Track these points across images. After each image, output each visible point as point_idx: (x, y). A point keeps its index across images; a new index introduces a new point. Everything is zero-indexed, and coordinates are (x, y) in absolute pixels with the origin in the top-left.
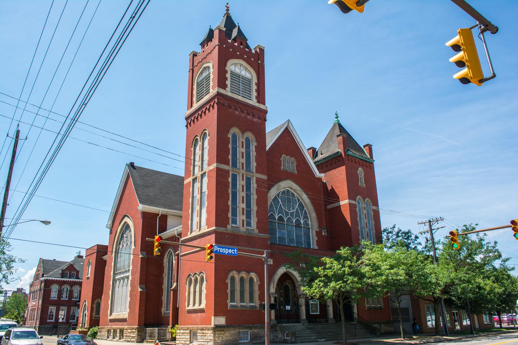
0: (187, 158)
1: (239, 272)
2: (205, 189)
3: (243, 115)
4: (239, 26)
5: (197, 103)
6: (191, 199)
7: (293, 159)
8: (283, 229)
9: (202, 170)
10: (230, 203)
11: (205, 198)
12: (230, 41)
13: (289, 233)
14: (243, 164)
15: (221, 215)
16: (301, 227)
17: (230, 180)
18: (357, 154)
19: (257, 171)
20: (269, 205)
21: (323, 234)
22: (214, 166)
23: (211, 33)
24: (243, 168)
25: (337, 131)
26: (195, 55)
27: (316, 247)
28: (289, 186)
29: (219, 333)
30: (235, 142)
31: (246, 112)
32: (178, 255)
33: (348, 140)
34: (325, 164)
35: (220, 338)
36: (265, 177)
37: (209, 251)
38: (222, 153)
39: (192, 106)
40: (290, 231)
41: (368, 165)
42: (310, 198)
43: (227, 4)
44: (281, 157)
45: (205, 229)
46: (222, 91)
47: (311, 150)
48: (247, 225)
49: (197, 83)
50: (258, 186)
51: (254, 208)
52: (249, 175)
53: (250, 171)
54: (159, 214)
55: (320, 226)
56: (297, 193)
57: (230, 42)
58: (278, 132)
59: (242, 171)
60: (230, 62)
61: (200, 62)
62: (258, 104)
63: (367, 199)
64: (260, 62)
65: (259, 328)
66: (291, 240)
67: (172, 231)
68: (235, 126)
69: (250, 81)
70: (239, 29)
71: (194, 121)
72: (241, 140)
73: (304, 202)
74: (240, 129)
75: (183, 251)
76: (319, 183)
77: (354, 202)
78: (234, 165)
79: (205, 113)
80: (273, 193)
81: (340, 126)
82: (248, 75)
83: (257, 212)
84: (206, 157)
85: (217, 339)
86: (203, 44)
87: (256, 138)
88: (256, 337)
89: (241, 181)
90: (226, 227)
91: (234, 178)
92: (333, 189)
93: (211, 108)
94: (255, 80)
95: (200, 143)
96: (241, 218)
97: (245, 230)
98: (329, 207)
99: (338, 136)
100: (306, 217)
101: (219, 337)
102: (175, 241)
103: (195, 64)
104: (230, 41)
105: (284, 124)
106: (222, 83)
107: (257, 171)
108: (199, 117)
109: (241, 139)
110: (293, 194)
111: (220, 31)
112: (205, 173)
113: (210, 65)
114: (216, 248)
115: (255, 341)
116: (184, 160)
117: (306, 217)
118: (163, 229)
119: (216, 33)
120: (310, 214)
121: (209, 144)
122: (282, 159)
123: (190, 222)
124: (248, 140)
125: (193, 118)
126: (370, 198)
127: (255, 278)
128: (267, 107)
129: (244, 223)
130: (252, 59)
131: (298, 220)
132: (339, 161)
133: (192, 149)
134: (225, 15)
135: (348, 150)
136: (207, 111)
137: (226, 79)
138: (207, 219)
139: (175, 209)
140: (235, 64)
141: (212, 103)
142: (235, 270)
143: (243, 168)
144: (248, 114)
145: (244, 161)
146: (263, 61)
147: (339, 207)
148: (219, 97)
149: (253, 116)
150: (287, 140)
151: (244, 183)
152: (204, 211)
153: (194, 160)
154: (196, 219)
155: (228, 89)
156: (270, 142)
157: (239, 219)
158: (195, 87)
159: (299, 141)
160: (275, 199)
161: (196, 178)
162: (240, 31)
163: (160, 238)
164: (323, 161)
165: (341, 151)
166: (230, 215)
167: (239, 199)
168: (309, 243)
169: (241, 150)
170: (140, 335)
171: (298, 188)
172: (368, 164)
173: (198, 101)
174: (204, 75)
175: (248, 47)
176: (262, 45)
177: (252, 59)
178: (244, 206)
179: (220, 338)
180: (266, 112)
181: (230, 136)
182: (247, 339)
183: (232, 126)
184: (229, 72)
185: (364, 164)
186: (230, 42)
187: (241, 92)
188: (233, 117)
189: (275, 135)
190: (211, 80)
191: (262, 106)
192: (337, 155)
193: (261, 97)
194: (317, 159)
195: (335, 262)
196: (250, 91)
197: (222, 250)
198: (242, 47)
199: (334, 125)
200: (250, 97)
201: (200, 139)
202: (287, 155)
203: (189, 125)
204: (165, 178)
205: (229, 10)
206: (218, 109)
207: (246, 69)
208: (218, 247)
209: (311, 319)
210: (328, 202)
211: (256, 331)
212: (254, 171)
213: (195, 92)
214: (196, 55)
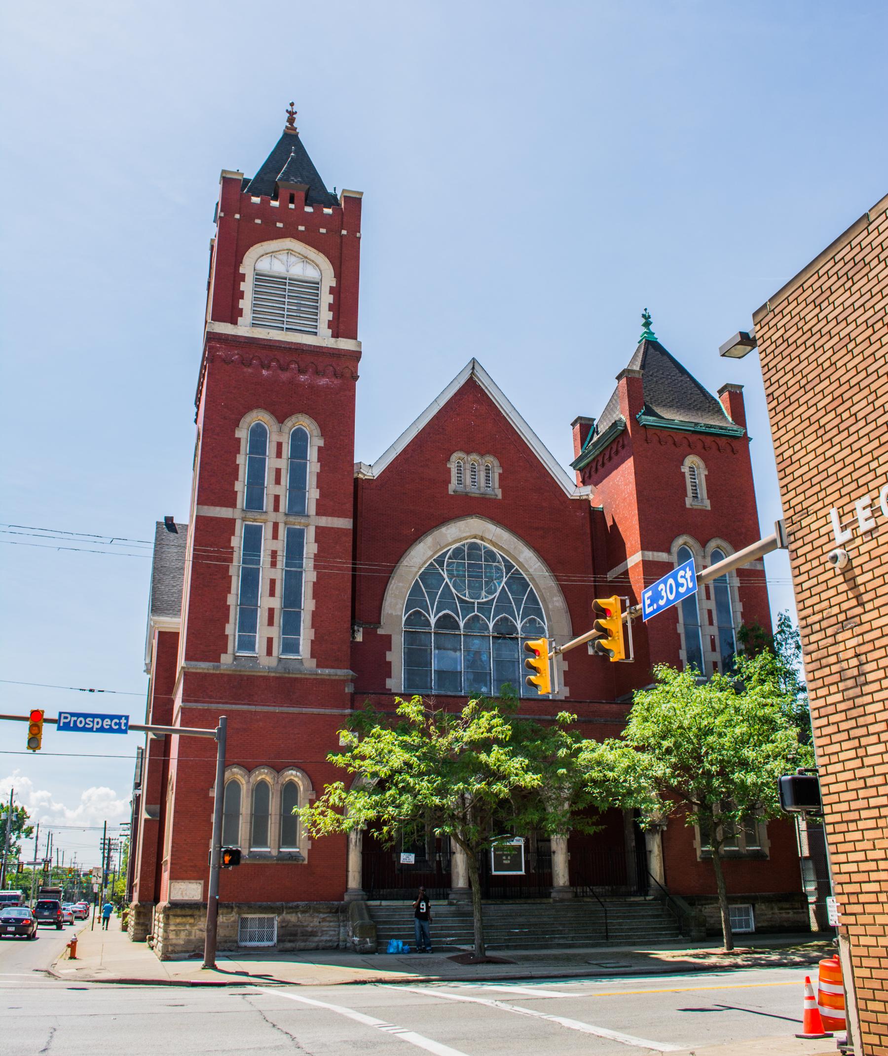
1: (249, 769)
3: (284, 376)
7: (490, 460)
8: (455, 650)
16: (517, 638)
28: (473, 532)
29: (178, 920)
35: (183, 935)
40: (478, 653)
43: (292, 104)
52: (297, 523)
57: (284, 197)
64: (344, 232)
65: (303, 912)
68: (258, 407)
74: (273, 413)
76: (580, 514)
78: (255, 502)
82: (311, 273)
83: (315, 615)
85: (172, 936)
88: (295, 935)
90: (218, 660)
92: (614, 526)
94: (329, 280)
101: (177, 933)
115: (289, 945)
127: (300, 783)
128: (360, 344)
130: (323, 231)
142: (239, 765)
144: (301, 371)
165: (625, 418)
170: (143, 924)
172: (722, 442)
179: (183, 935)
180: (356, 356)
182: (272, 940)
183: (249, 409)
193: (345, 319)
198: (292, 206)
202: (468, 453)
207: (305, 259)
209: (490, 887)
211: (292, 918)
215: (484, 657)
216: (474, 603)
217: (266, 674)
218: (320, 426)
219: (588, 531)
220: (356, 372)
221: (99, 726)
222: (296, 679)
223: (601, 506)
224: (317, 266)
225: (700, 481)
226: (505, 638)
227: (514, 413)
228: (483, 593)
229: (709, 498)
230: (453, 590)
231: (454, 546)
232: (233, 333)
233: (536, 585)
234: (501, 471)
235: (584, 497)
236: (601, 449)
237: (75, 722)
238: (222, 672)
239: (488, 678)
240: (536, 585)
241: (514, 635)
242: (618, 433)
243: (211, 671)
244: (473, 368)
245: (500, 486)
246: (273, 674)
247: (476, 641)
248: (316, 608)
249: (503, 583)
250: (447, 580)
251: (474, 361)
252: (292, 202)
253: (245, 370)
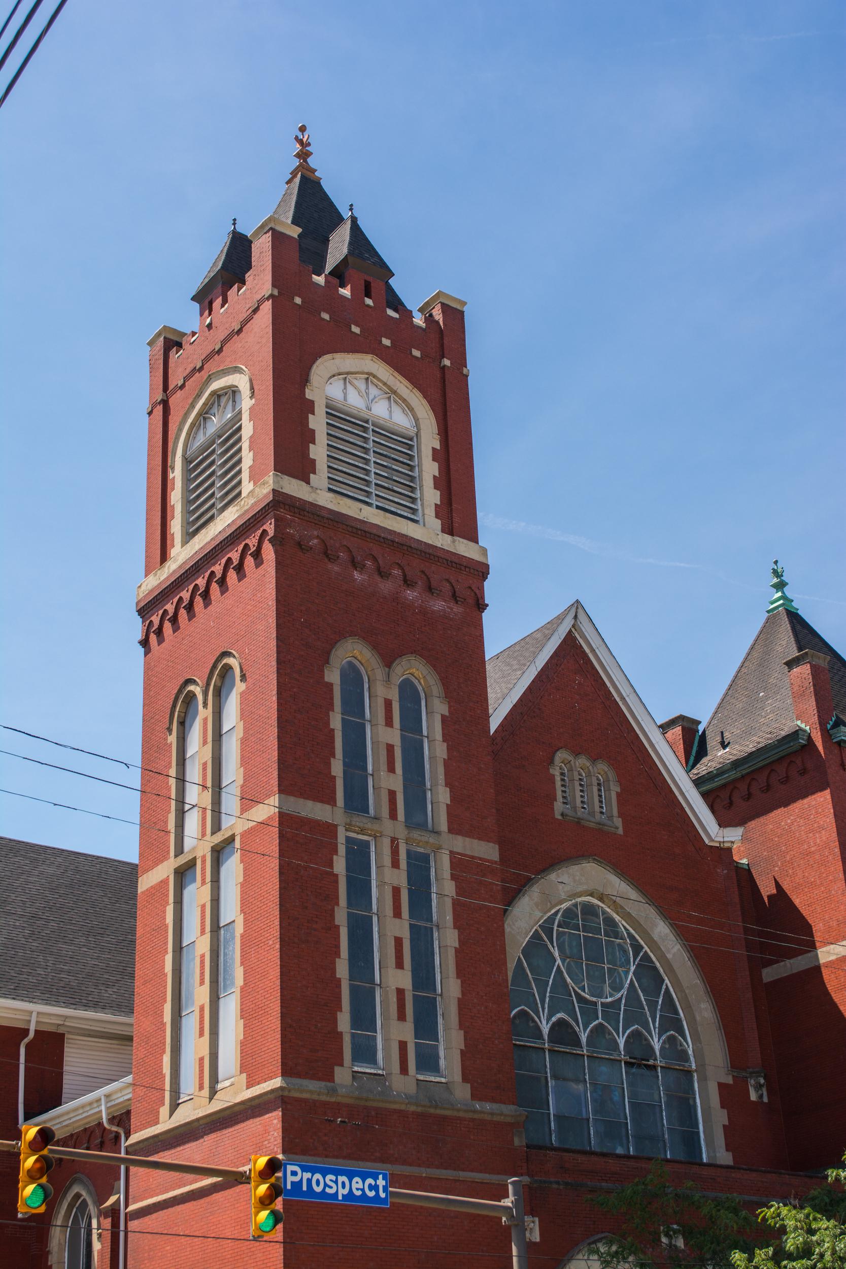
0: (151, 770)
2: (231, 910)
3: (386, 587)
4: (354, 220)
5: (185, 543)
6: (169, 959)
8: (577, 1081)
9: (217, 827)
10: (342, 969)
11: (234, 952)
12: (320, 280)
13: (603, 1093)
14: (392, 794)
15: (308, 1027)
16: (654, 1067)
17: (340, 866)
19: (455, 828)
20: (510, 974)
21: (753, 1096)
22: (268, 809)
23: (238, 256)
24: (393, 815)
26: (172, 342)
27: (725, 1158)
30: (354, 705)
31: (396, 572)
32: (114, 1212)
36: (488, 851)
37: (263, 1188)
38: (304, 752)
39: (164, 557)
43: (303, 129)
44: (551, 761)
45: (235, 1090)
46: (293, 488)
47: (678, 730)
48: (420, 1068)
49: (187, 461)
50: (460, 890)
51: (449, 986)
52: (422, 842)
53: (422, 826)
54: (26, 1032)
55: (737, 1061)
56: (627, 916)
57: (320, 279)
58: (535, 655)
59: (388, 827)
60: (324, 367)
61: (194, 371)
62: (448, 538)
64: (447, 362)
66: (613, 1129)
67: (84, 1103)
68: (353, 634)
69: (407, 443)
70: (356, 229)
71: (174, 620)
72: (382, 692)
73: (662, 957)
74: (375, 647)
75: (146, 1188)
76: (722, 871)
78: (357, 801)
79: (222, 582)
80: (525, 918)
81: (795, 619)
82: (401, 420)
83: (463, 1005)
84: (232, 773)
86: (205, 298)
87: (445, 682)
89: (388, 872)
90: (330, 1077)
91: (359, 857)
92: (781, 895)
93: (249, 561)
94: (430, 440)
95: (204, 713)
96: (391, 1033)
97: (412, 1089)
98: (769, 974)
99: (790, 664)
100: (671, 1023)
102: (101, 1147)
103: (176, 379)
104: (320, 280)
105: (560, 619)
106: (291, 456)
107: (455, 828)
108: (198, 600)
109: (380, 690)
110: (610, 922)
111: (278, 238)
112: (231, 840)
113: (241, 381)
114: (294, 1174)
116: (134, 778)
117: (671, 1023)
118: (46, 1095)
119: (262, 252)
120: (688, 1008)
121: (244, 715)
122: (555, 772)
123: (167, 1059)
124: (409, 694)
125: (170, 607)
128: (484, 551)
129: (407, 1056)
130: (416, 353)
131: (636, 1035)
132: (803, 772)
133: (172, 739)
134: (294, 174)
136: (232, 575)
137: (310, 437)
138: (243, 1044)
139: (96, 1005)
140: (346, 376)
141: (252, 542)
143: (393, 815)
144: (408, 583)
145: (396, 782)
146: (461, 360)
147: (816, 971)
148: (281, 512)
149: (430, 589)
151: (400, 878)
152: (230, 1007)
153: (181, 780)
154: (194, 1047)
155: (320, 478)
156: (503, 697)
157: (386, 1040)
158: (177, 474)
159: (625, 691)
160: (536, 947)
161: (192, 864)
162: (358, 237)
163: (45, 1136)
164: (733, 775)
165: (808, 725)
166: (344, 1022)
167: (381, 951)
168: (690, 1140)
169: (381, 736)
173: (189, 535)
174: (215, 423)
175: (395, 303)
176: (454, 291)
177: (416, 353)
178: (404, 979)
180: (481, 571)
181: (333, 676)
184: (320, 409)
186: (320, 279)
187: (372, 489)
188: (346, 594)
190: (245, 445)
191: (463, 548)
193: (458, 512)
195: (824, 1224)
196: (411, 484)
197: (321, 1183)
198: (369, 302)
199: (772, 619)
201: (205, 694)
202: (577, 754)
203: (153, 638)
204: (51, 870)
205: (309, 154)
206: (279, 563)
207: (391, 394)
208: (304, 1169)
212: (444, 826)
213: (176, 497)
214: (179, 345)
215: (616, 1097)
216: (595, 1004)
217: (403, 1107)
220: (483, 598)
221: (346, 1191)
222: (444, 1118)
226: (639, 1066)
228: (607, 989)
230: (569, 980)
231: (564, 906)
232: (310, 500)
233: (676, 983)
234: (619, 790)
235: (726, 845)
237: (309, 1181)
238: (339, 1099)
239: (623, 1131)
240: (676, 983)
241: (651, 1062)
243: (324, 1098)
245: (621, 815)
246: (412, 1108)
247: (604, 1069)
248: (463, 993)
249: (631, 974)
250: (559, 961)
251: (578, 604)
252: (368, 295)
253: (330, 566)
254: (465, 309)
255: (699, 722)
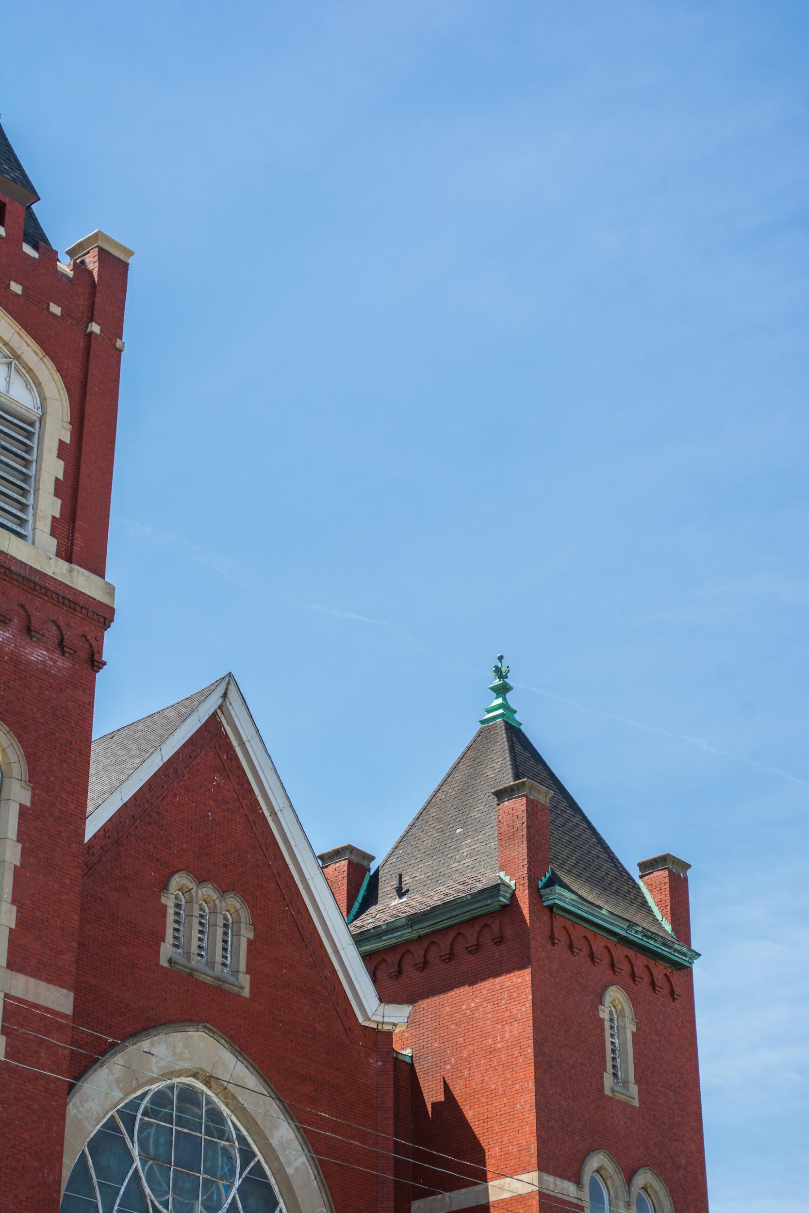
7: (233, 903)
18: (606, 910)
20: (66, 1174)
25: (500, 769)
33: (558, 829)
34: (418, 952)
36: (58, 999)
41: (662, 976)
42: (312, 1141)
47: (342, 865)
56: (239, 1110)
58: (163, 739)
62: (64, 565)
63: (644, 1177)
64: (95, 328)
73: (280, 1172)
77: (566, 1189)
80: (98, 1098)
81: (516, 737)
82: (21, 396)
94: (57, 428)
99: (501, 795)
105: (204, 695)
110: (215, 1116)
126: (661, 1172)
128: (111, 590)
130: (55, 309)
132: (500, 940)
135: (554, 881)
146: (115, 328)
149: (28, 630)
150: (210, 789)
156: (108, 794)
159: (278, 802)
160: (108, 1141)
164: (408, 934)
165: (514, 880)
171: (252, 1081)
175: (38, 238)
176: (122, 235)
177: (55, 309)
180: (104, 616)
185: (639, 970)
189: (144, 755)
191: (82, 581)
192: (492, 905)
193: (83, 530)
194: (369, 920)
200: (22, 522)
202: (201, 881)
210: (417, 1172)
218: (28, 756)
219: (390, 1103)
220: (100, 652)
223: (408, 1052)
224: (38, 385)
225: (624, 1043)
227: (288, 812)
229: (638, 1081)
231: (155, 1087)
234: (251, 936)
235: (387, 1028)
236: (422, 932)
242: (494, 907)
244: (225, 696)
245: (249, 970)
249: (234, 1191)
250: (137, 1163)
254: (130, 261)
255: (373, 858)
